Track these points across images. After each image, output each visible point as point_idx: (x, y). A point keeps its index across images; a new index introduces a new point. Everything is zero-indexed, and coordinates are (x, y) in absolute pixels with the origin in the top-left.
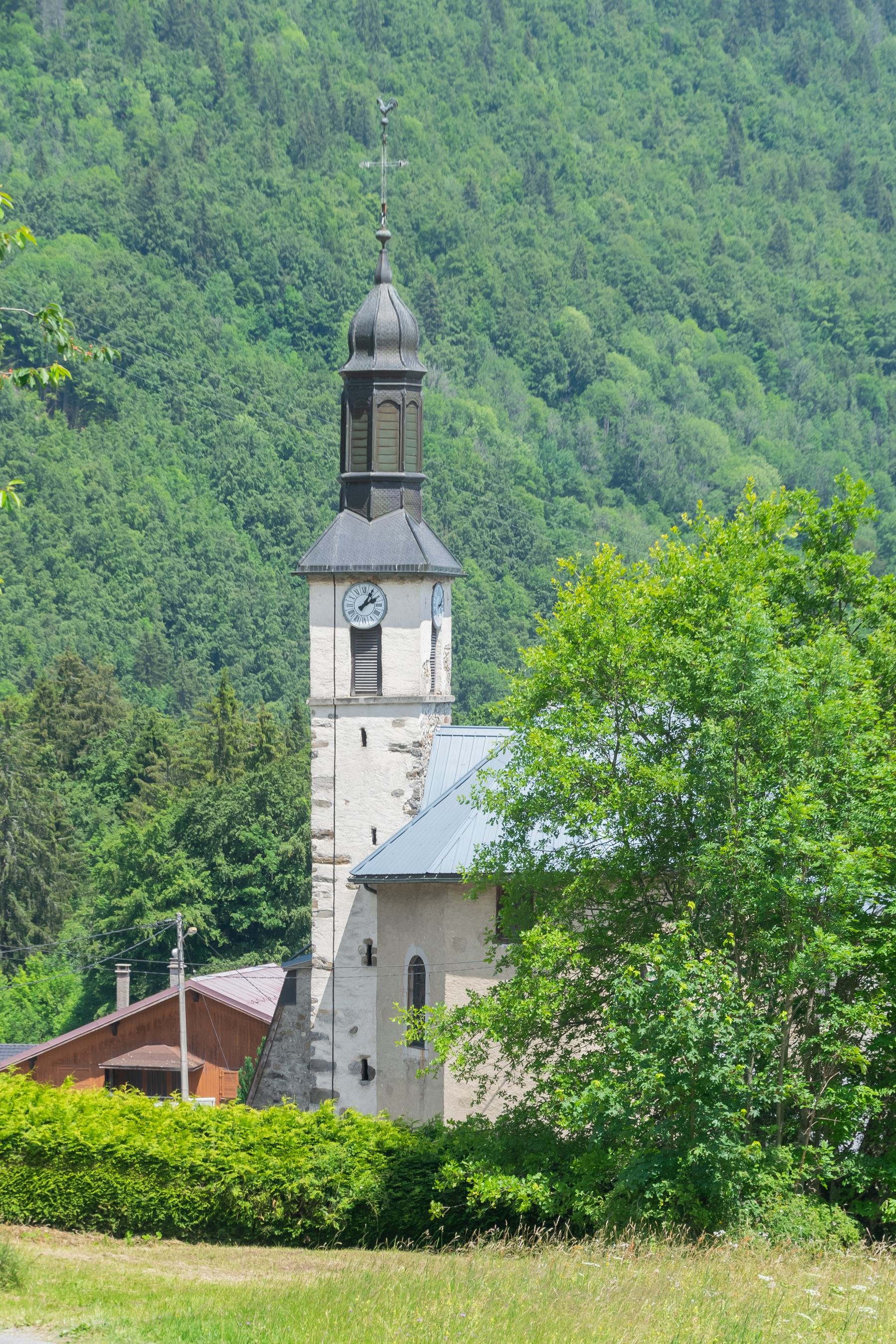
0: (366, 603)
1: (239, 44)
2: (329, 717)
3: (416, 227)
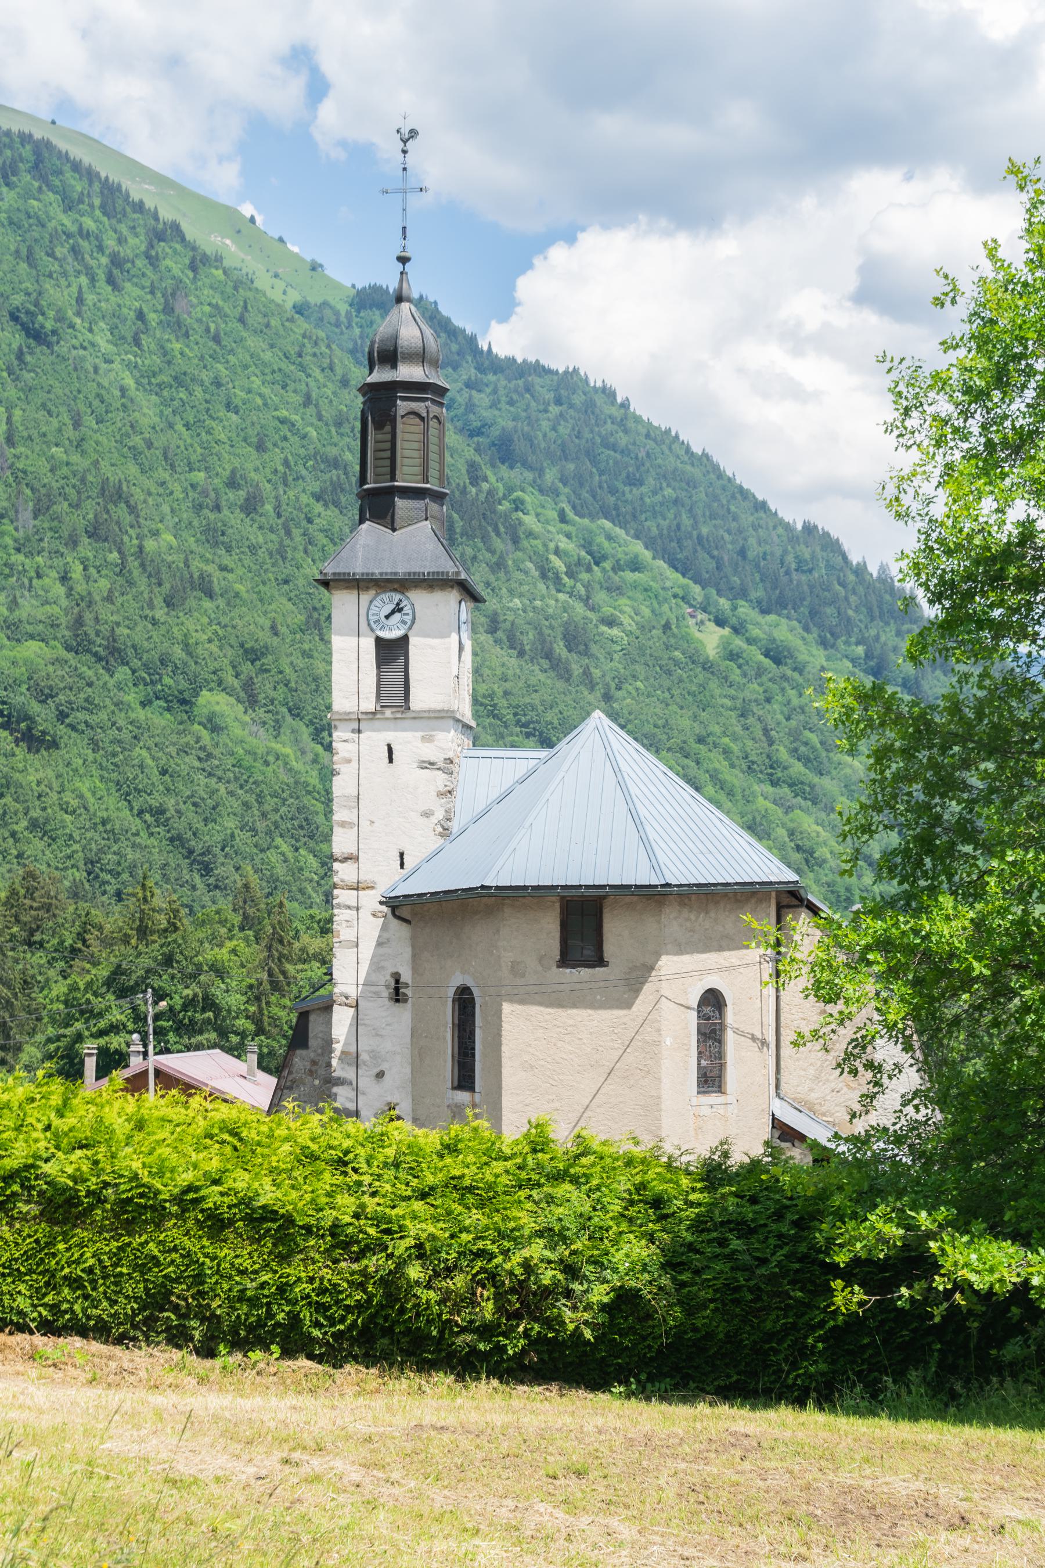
0: (393, 612)
1: (135, 542)
2: (353, 731)
3: (242, 645)
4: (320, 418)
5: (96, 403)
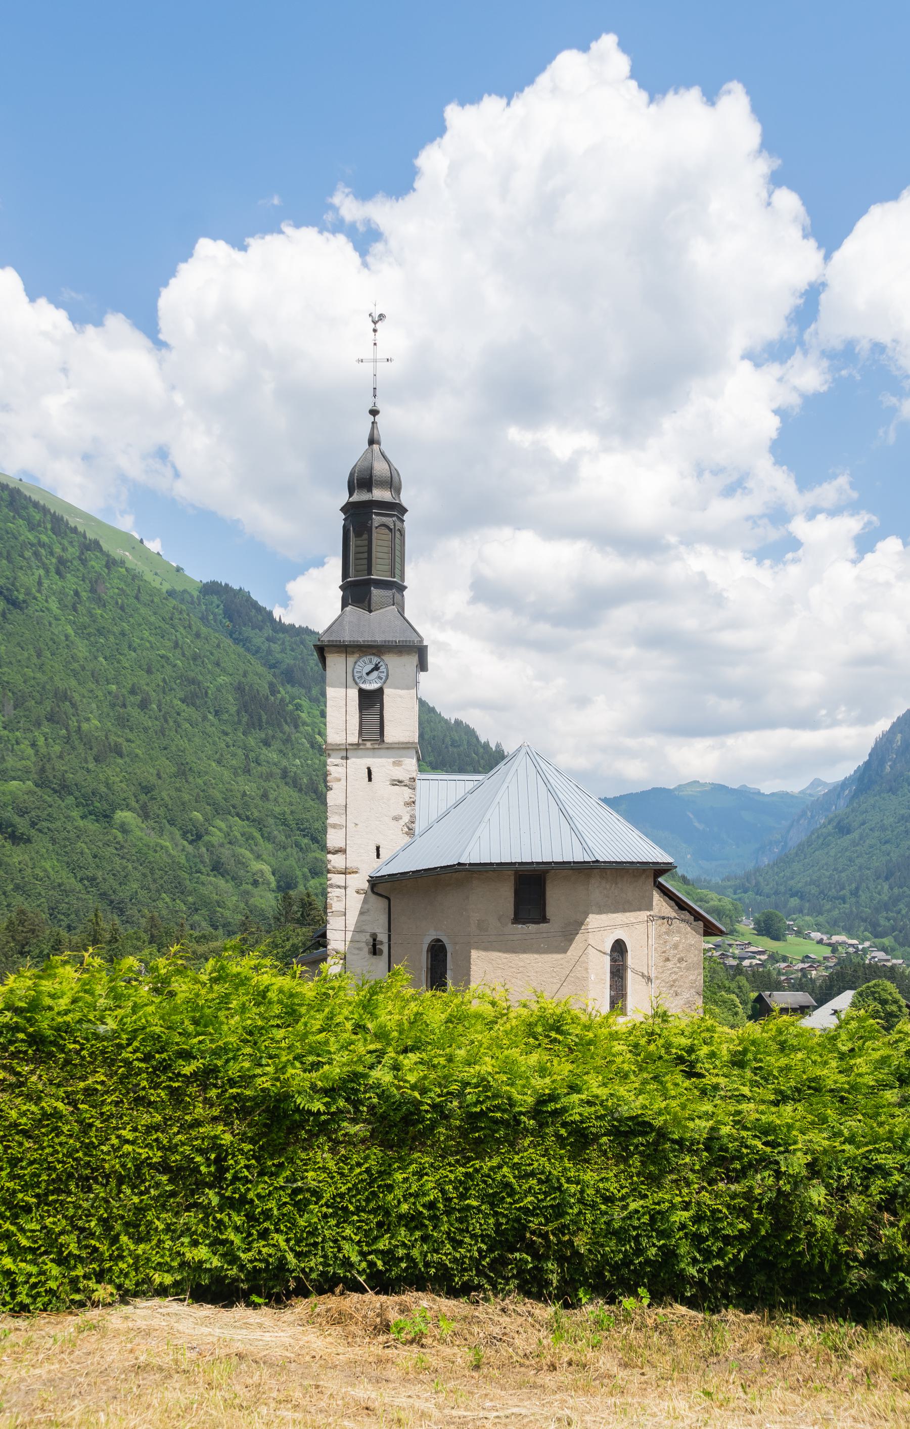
2: (342, 758)
4: (184, 655)
5: (50, 643)
